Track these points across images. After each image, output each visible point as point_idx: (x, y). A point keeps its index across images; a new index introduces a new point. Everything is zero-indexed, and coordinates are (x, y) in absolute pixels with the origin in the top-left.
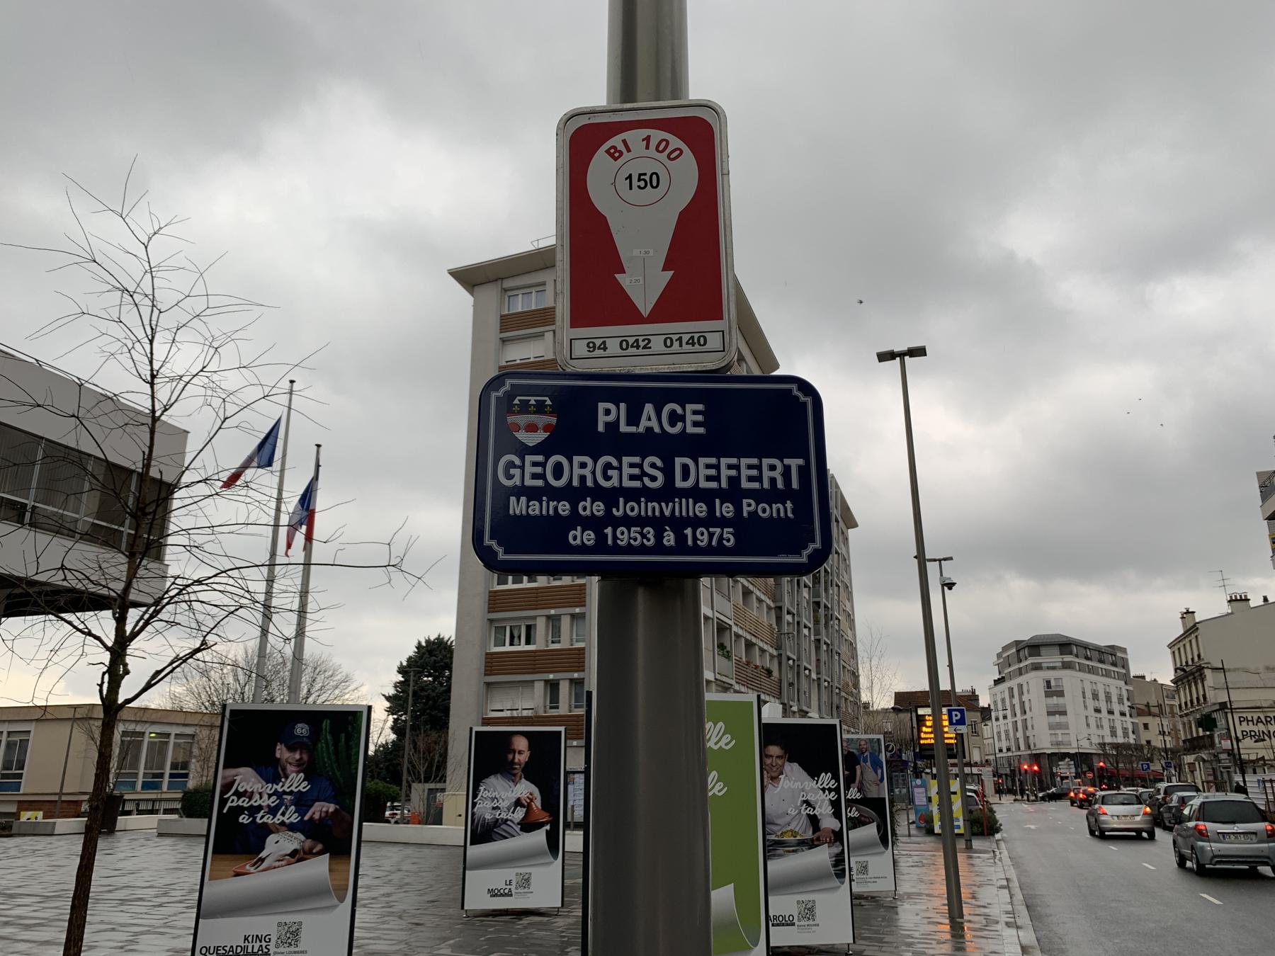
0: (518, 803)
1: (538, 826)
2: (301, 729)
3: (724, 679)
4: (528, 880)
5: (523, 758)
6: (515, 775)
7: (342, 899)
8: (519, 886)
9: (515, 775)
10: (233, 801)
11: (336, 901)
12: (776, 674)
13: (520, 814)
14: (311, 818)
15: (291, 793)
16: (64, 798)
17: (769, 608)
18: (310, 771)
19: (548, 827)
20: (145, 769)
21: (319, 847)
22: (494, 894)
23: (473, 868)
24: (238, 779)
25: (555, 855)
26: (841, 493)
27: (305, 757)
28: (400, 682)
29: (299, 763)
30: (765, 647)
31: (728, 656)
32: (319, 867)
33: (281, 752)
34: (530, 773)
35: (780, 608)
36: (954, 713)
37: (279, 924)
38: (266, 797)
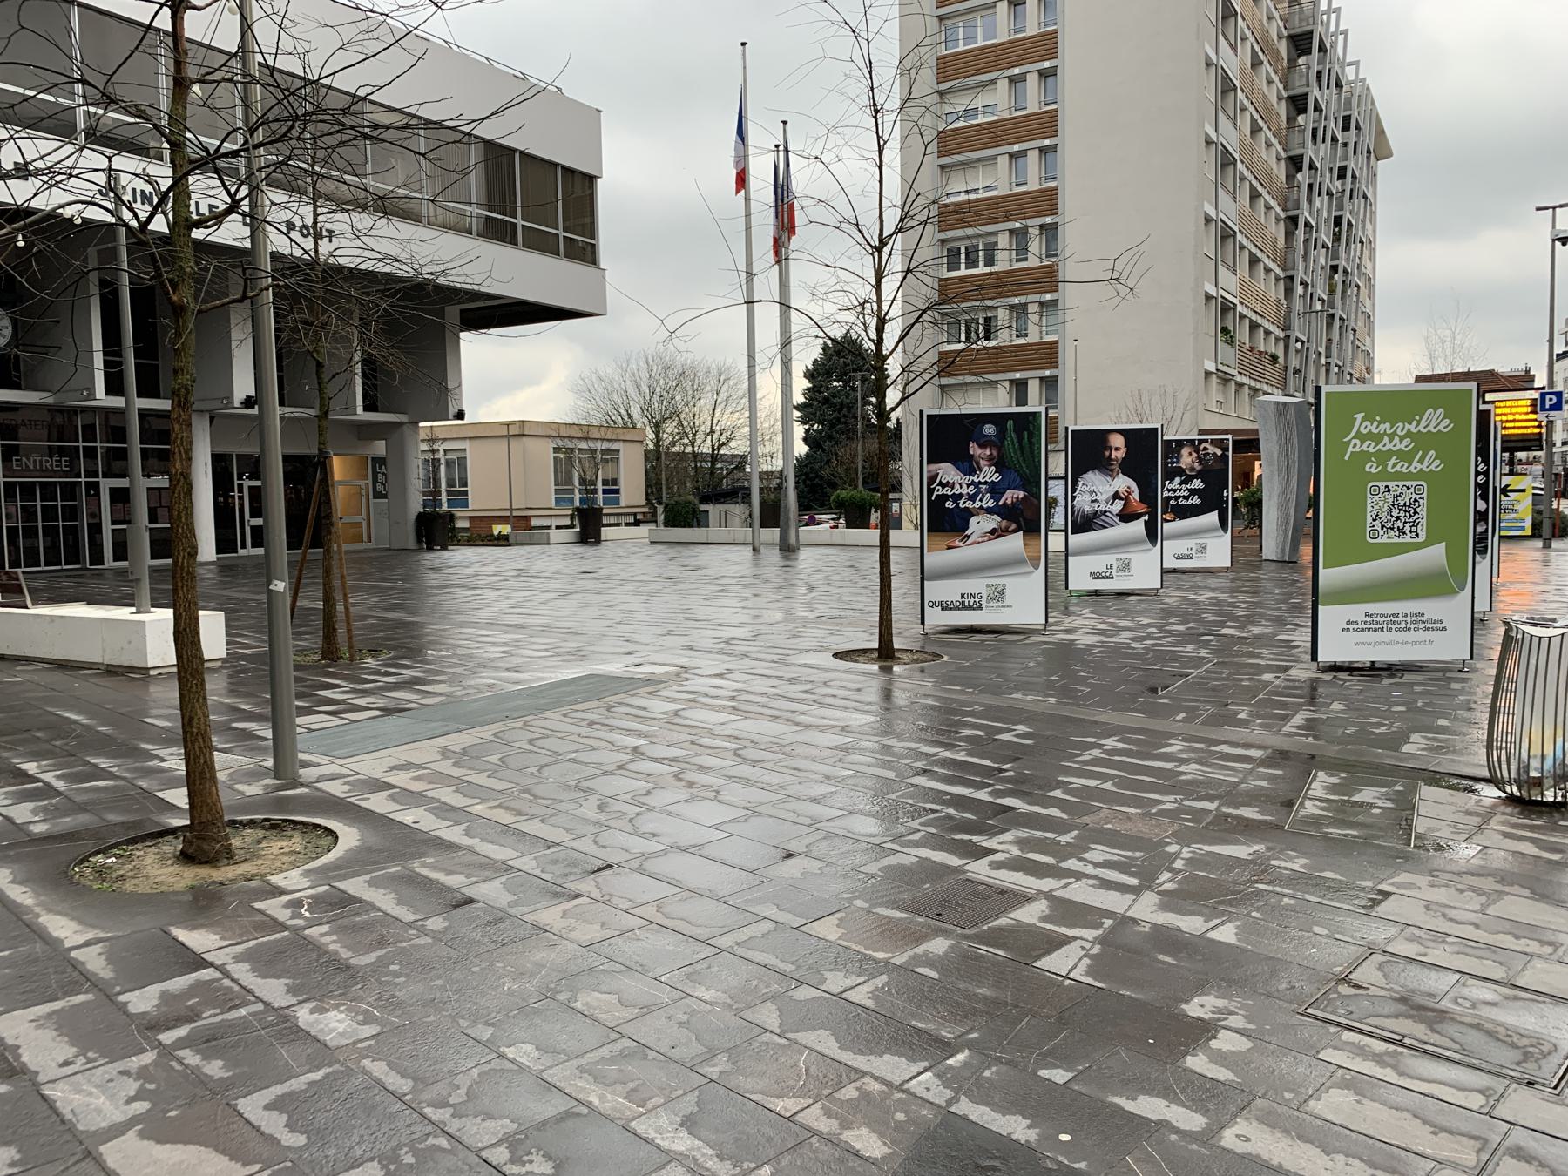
0: (1116, 496)
1: (1137, 516)
2: (989, 429)
3: (1226, 369)
4: (1128, 565)
5: (1119, 455)
6: (1112, 470)
7: (1036, 567)
8: (1119, 569)
9: (1112, 470)
10: (1355, 445)
11: (1032, 569)
12: (1281, 360)
13: (1118, 505)
14: (1005, 503)
15: (986, 483)
16: (515, 513)
17: (1278, 279)
18: (999, 464)
19: (1146, 518)
20: (153, 519)
21: (1014, 526)
22: (1096, 576)
23: (1075, 554)
24: (941, 472)
25: (1225, 530)
26: (1378, 115)
27: (995, 453)
28: (808, 389)
29: (990, 458)
30: (1271, 328)
31: (1230, 342)
32: (1014, 543)
33: (973, 449)
34: (1127, 468)
35: (1291, 278)
36: (1548, 397)
37: (987, 586)
38: (965, 486)
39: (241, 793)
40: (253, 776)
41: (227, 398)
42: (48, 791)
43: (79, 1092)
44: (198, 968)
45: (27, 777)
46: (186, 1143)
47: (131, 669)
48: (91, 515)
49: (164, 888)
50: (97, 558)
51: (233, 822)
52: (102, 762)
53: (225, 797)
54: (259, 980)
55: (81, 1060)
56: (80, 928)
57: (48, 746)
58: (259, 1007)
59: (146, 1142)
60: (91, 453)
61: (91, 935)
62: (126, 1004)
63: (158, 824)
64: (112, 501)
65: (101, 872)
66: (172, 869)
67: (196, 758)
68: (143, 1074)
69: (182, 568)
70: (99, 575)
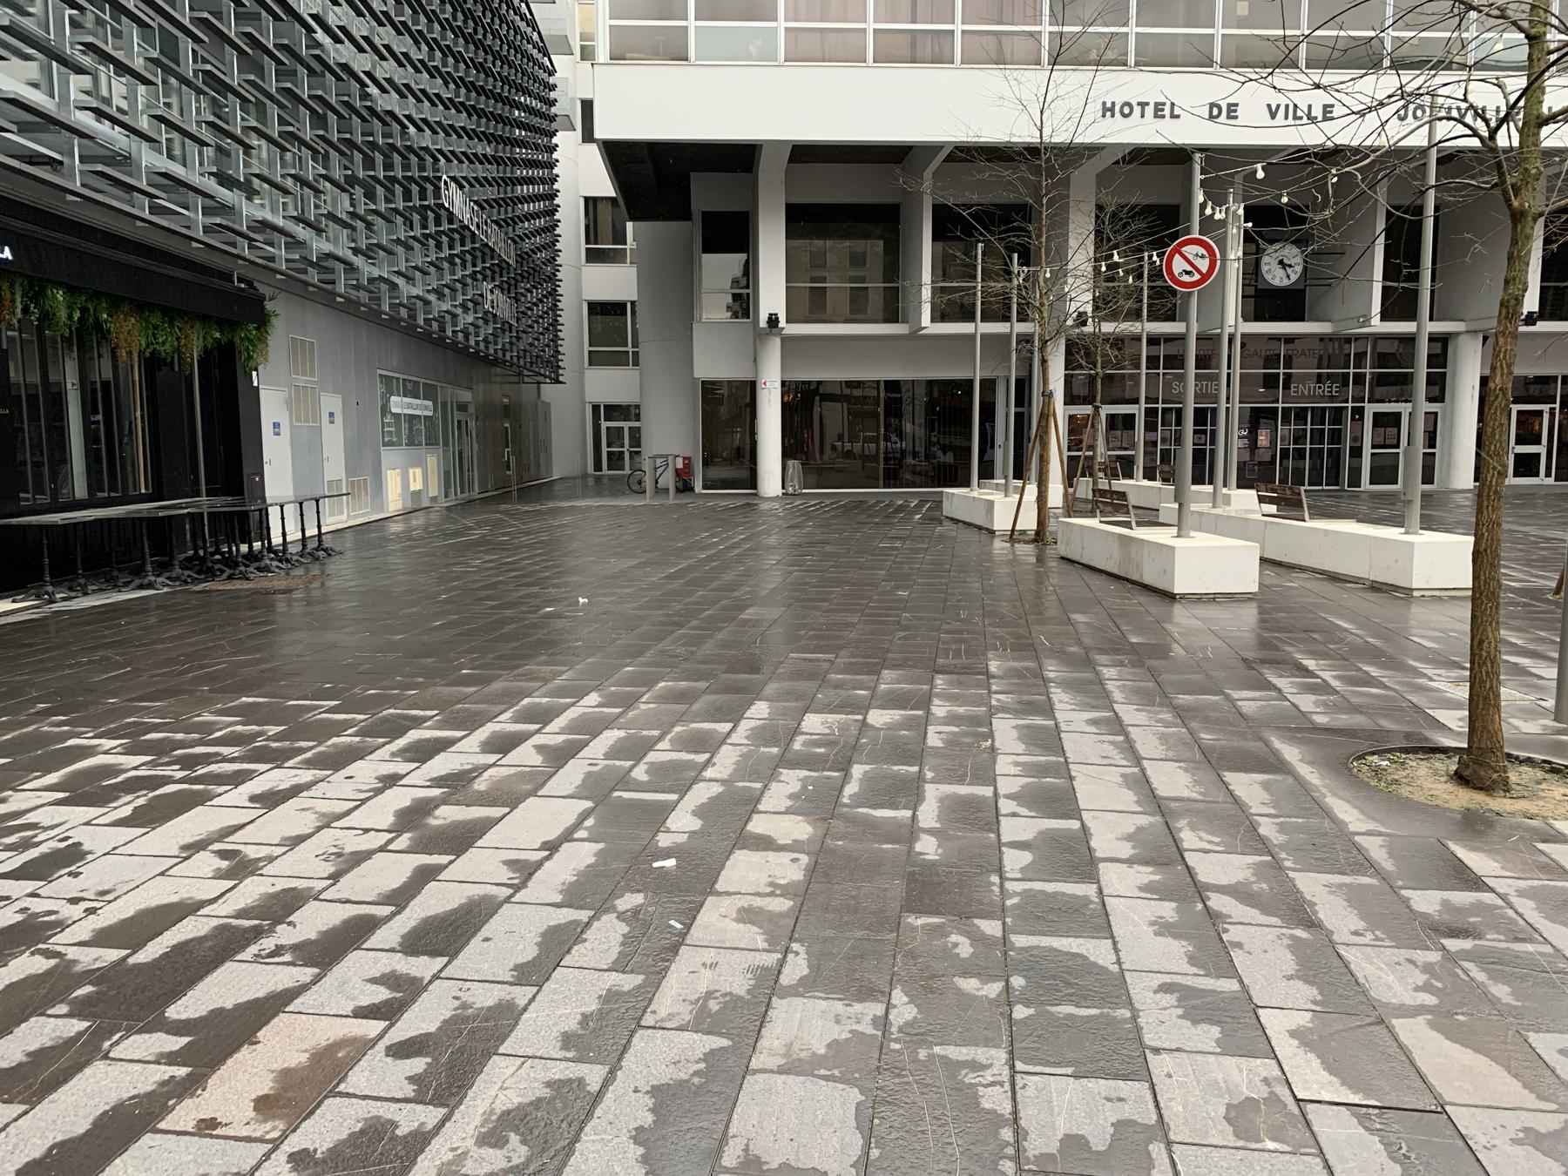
39: (1517, 728)
40: (1532, 713)
41: (1364, 316)
42: (1325, 688)
43: (1371, 963)
44: (1478, 889)
45: (1306, 672)
46: (1477, 1051)
47: (1396, 588)
48: (1354, 439)
49: (1438, 802)
50: (1355, 481)
51: (1509, 756)
52: (1374, 671)
53: (1507, 732)
54: (1546, 922)
55: (1369, 936)
56: (1362, 817)
57: (1322, 647)
58: (1548, 949)
59: (1435, 1033)
60: (1359, 379)
61: (1372, 826)
62: (1408, 899)
63: (1427, 740)
64: (1375, 425)
65: (1377, 772)
66: (1445, 786)
67: (1482, 682)
68: (1427, 968)
69: (1490, 488)
70: (1356, 496)
